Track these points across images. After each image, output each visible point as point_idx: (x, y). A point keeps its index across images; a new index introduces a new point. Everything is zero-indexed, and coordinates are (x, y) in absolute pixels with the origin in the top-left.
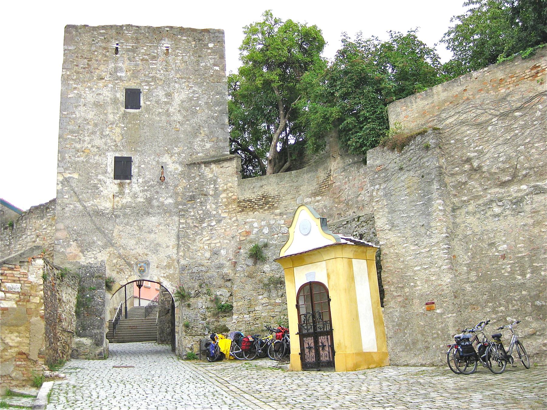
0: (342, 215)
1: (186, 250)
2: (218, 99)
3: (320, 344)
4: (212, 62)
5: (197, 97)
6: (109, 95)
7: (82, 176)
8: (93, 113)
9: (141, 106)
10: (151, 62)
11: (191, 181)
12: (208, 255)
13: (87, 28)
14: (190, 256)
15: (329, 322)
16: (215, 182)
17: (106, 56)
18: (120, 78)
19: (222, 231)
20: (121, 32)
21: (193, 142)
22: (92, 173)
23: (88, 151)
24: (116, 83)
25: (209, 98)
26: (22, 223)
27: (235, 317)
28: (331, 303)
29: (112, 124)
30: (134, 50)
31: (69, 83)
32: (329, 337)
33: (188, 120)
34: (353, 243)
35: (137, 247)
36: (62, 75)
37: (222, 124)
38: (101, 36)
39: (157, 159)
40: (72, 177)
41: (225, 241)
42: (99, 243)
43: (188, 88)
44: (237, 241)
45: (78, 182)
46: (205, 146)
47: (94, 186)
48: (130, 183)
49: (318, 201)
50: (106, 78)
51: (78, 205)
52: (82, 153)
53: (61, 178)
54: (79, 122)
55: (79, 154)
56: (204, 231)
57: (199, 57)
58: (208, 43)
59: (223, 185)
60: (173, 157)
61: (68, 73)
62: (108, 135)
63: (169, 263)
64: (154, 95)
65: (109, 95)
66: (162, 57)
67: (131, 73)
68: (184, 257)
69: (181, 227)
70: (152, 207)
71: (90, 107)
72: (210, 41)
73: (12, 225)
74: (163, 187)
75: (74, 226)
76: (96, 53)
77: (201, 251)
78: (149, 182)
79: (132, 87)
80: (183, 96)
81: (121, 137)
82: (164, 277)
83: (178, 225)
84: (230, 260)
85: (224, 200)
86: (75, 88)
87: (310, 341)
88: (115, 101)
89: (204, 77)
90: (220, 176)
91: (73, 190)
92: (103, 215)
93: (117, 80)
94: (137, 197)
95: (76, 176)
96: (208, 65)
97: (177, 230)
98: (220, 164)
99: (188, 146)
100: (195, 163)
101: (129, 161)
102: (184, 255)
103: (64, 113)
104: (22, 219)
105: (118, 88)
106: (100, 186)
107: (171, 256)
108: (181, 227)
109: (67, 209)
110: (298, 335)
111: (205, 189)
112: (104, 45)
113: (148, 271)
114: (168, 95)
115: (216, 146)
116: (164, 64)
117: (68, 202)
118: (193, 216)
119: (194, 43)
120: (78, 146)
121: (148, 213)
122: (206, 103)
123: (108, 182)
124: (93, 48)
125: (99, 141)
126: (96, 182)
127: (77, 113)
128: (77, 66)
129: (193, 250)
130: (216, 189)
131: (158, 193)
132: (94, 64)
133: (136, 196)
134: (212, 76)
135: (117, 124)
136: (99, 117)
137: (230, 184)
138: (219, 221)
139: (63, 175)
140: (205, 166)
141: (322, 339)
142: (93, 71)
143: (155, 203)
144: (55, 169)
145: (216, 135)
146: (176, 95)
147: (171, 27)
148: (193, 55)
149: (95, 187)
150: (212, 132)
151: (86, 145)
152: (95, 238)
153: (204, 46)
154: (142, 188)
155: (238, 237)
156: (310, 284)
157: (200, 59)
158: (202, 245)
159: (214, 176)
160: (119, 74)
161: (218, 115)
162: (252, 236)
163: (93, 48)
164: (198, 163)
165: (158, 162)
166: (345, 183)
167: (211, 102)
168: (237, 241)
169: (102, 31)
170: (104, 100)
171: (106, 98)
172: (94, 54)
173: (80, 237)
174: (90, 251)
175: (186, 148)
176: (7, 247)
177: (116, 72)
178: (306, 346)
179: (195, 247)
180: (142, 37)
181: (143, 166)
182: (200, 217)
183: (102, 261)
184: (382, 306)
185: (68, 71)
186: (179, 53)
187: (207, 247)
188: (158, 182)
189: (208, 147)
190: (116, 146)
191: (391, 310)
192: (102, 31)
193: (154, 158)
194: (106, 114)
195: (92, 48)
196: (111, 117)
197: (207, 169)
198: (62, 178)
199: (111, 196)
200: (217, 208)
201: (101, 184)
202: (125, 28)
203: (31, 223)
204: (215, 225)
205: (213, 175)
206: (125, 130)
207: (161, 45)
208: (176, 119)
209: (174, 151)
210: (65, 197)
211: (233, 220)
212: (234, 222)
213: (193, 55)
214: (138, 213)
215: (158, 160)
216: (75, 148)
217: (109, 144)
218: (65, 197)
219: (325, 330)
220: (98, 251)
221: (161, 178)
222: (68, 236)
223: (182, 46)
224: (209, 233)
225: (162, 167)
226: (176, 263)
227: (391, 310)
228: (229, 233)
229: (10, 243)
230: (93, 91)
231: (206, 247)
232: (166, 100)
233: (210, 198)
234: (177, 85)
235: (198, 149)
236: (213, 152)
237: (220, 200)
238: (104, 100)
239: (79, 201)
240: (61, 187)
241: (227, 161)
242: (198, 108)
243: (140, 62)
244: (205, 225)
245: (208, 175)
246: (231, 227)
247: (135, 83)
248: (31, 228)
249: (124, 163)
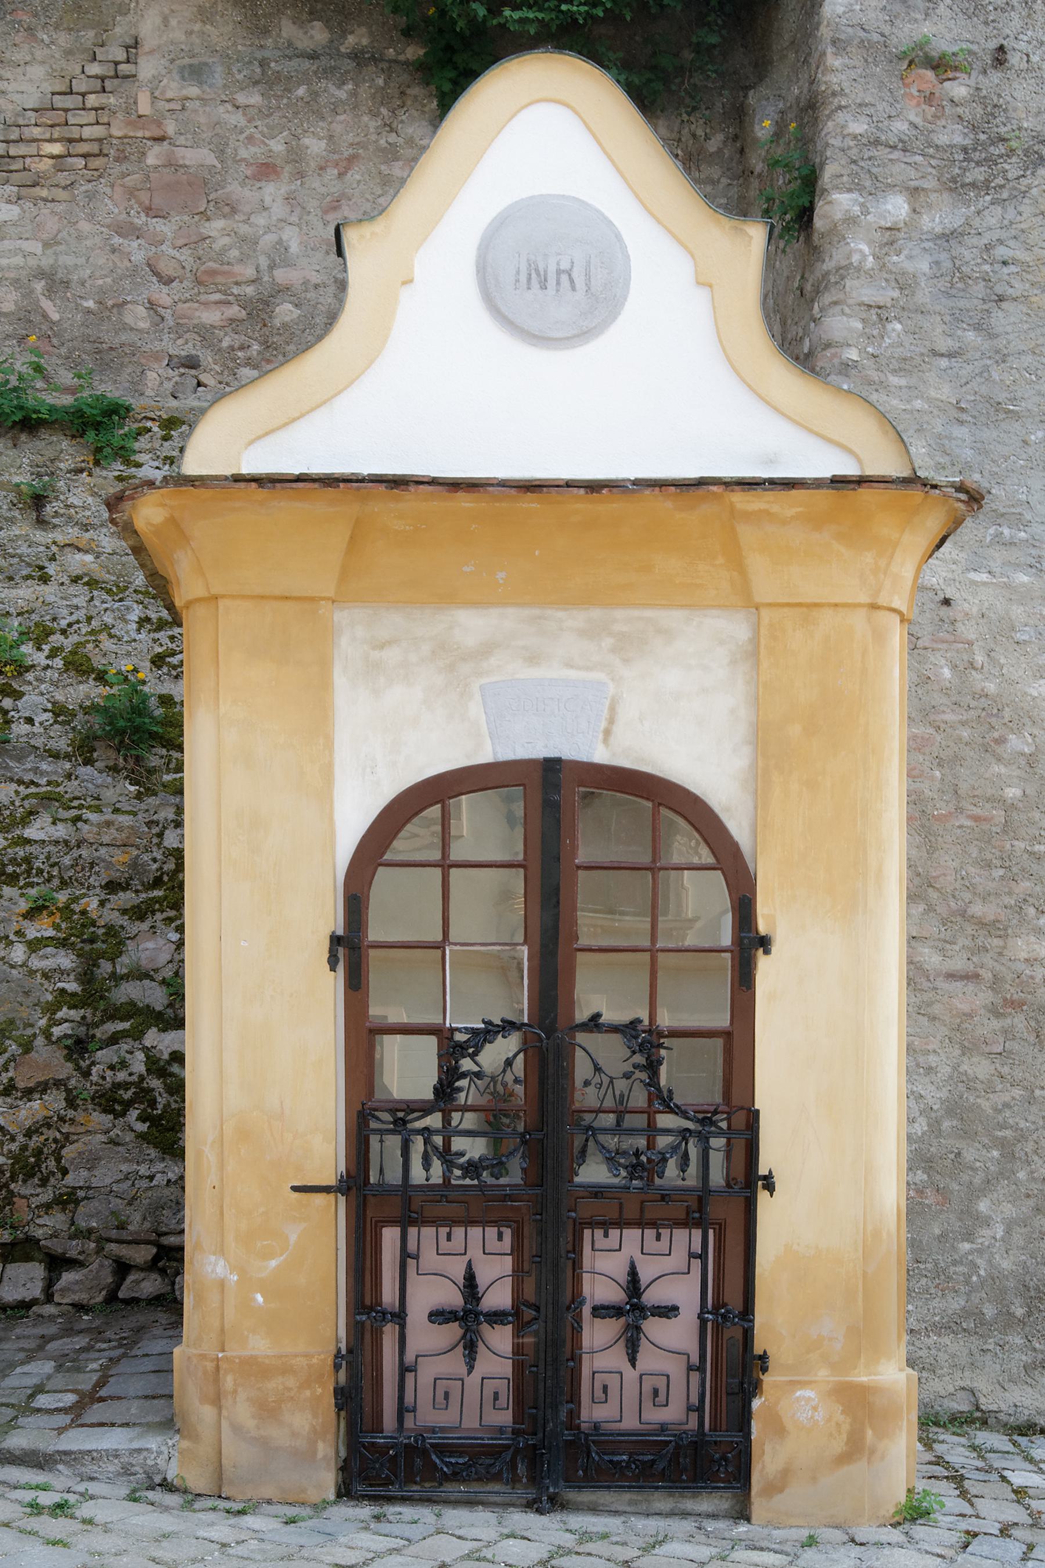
166: (266, 170)
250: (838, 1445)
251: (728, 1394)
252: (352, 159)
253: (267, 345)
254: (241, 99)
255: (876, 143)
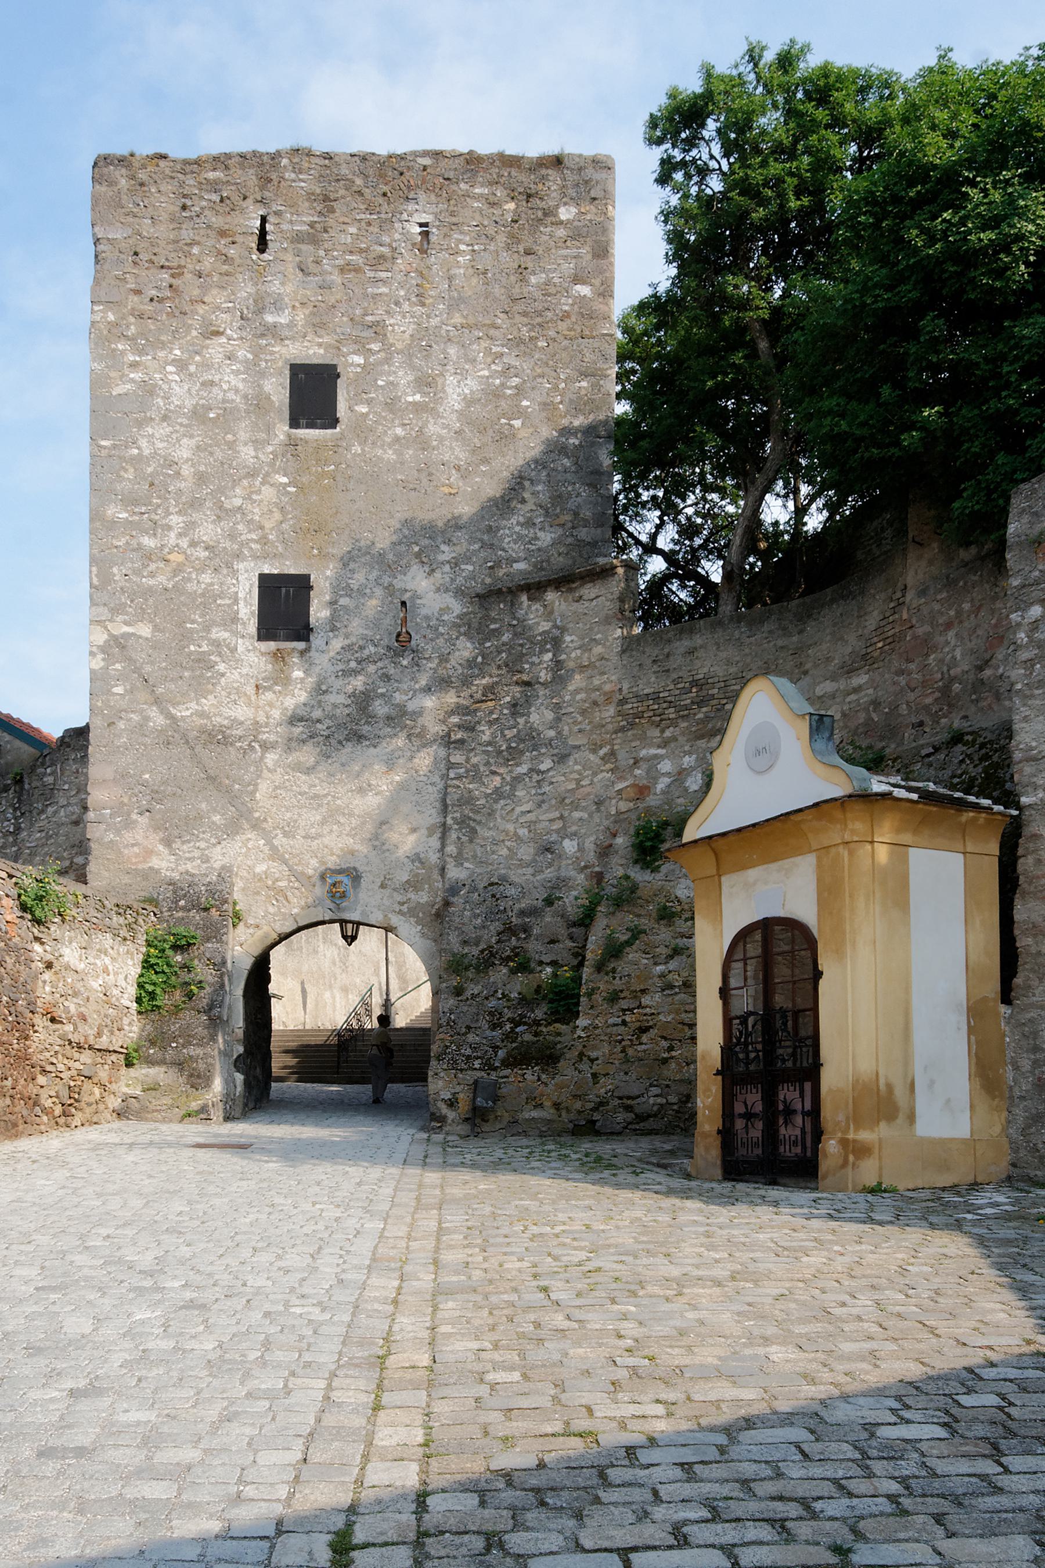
0: (927, 729)
1: (464, 839)
2: (583, 392)
3: (781, 1107)
4: (568, 268)
5: (516, 387)
6: (241, 386)
7: (162, 631)
8: (193, 442)
9: (337, 421)
10: (371, 274)
11: (488, 644)
12: (526, 852)
13: (162, 163)
14: (475, 856)
15: (809, 1042)
16: (557, 643)
17: (227, 259)
18: (272, 331)
19: (570, 787)
20: (274, 176)
21: (498, 529)
22: (193, 622)
23: (180, 558)
24: (261, 347)
25: (556, 388)
26: (45, 774)
27: (582, 1022)
28: (823, 984)
29: (252, 474)
30: (313, 237)
31: (114, 350)
32: (808, 1086)
33: (485, 461)
34: (914, 796)
35: (326, 829)
36: (93, 323)
37: (592, 473)
38: (209, 191)
39: (386, 580)
40: (133, 634)
41: (577, 815)
42: (217, 818)
43: (489, 360)
44: (608, 815)
45: (151, 647)
46: (536, 538)
47: (199, 661)
48: (307, 650)
49: (856, 690)
50: (229, 332)
51: (154, 712)
52: (161, 565)
53: (101, 638)
54: (150, 470)
55: (153, 567)
56: (520, 786)
57: (528, 252)
58: (557, 207)
59: (579, 652)
60: (438, 575)
61: (111, 317)
62: (240, 508)
63: (417, 875)
64: (380, 383)
65: (241, 386)
66: (408, 258)
67: (307, 312)
68: (459, 860)
69: (452, 775)
70: (370, 718)
71: (181, 425)
72: (565, 198)
73: (19, 781)
74: (405, 663)
75: (143, 773)
76: (195, 250)
77: (508, 843)
78: (362, 648)
79: (308, 356)
80: (471, 385)
81: (277, 516)
82: (401, 912)
83: (444, 772)
84: (586, 867)
85: (578, 697)
86: (134, 365)
87: (753, 1099)
88: (259, 404)
89: (539, 320)
90: (571, 625)
91: (137, 670)
92: (225, 741)
93: (263, 335)
94: (325, 692)
95: (145, 630)
96: (556, 280)
97: (441, 785)
98: (571, 590)
99: (481, 540)
100: (499, 592)
101: (302, 584)
102: (460, 853)
103: (104, 443)
104: (43, 764)
105: (266, 361)
106: (218, 659)
107: (422, 856)
108: (452, 775)
109: (121, 725)
110: (720, 1078)
111: (526, 666)
112: (217, 221)
113: (356, 896)
114: (425, 383)
115: (570, 540)
116: (414, 282)
117: (123, 704)
118: (489, 744)
119: (511, 206)
120: (149, 542)
121: (360, 738)
122: (545, 404)
123: (240, 649)
124: (187, 234)
125: (211, 526)
126: (205, 648)
127: (143, 443)
128: (138, 292)
129: (484, 839)
130: (558, 664)
131: (389, 680)
132: (190, 287)
133: (324, 688)
134: (566, 315)
135: (267, 474)
136: (211, 454)
137: (598, 650)
138: (561, 759)
139: (106, 628)
140: (529, 599)
141: (788, 1094)
142: (187, 308)
143: (380, 708)
144: (84, 612)
145: (571, 504)
146: (451, 380)
147: (437, 155)
148: (508, 248)
149: (203, 662)
150: (558, 498)
151: (172, 538)
152: (204, 805)
153: (545, 214)
154: (341, 666)
155: (614, 801)
156: (766, 926)
157: (529, 261)
158: (510, 827)
159: (555, 626)
160: (270, 318)
161: (580, 445)
162: (652, 801)
163: (187, 234)
164: (510, 591)
165: (390, 590)
166: (949, 626)
167: (561, 402)
168: (608, 815)
169: (211, 175)
170: (224, 401)
171: (231, 395)
172: (188, 255)
173: (160, 802)
174: (189, 841)
175: (477, 546)
176: (11, 839)
177: (260, 311)
178: (739, 1108)
179: (491, 833)
180: (342, 192)
181: (343, 601)
182: (509, 748)
183: (223, 867)
184: (1006, 998)
185: (111, 309)
186: (460, 241)
187: (526, 831)
188: (389, 648)
189: (545, 544)
190: (264, 541)
191: (1032, 1014)
192: (211, 175)
193: (380, 577)
194: (231, 445)
195: (184, 232)
196: (247, 453)
197: (536, 606)
198: (106, 636)
199: (250, 690)
200: (558, 719)
201: (220, 655)
202: (285, 161)
203: (67, 773)
204: (548, 770)
205: (550, 624)
206: (289, 493)
207: (405, 216)
208: (446, 457)
209: (441, 557)
210: (115, 690)
211: (602, 752)
212: (602, 759)
213: (508, 248)
214: (328, 737)
215: (391, 585)
216: (140, 547)
217: (243, 537)
218: (115, 690)
219: (798, 1064)
220: (213, 841)
221: (399, 635)
222: (126, 800)
223: (473, 218)
224: (533, 792)
225: (403, 604)
226: (436, 876)
227: (1032, 1014)
228: (588, 789)
229: (18, 829)
230: (191, 375)
231: (523, 832)
232: (418, 397)
233: (541, 693)
234: (452, 351)
235: (515, 549)
236: (561, 559)
237: (567, 698)
238: (224, 401)
239: (157, 701)
240: (102, 664)
241: (592, 581)
242: (517, 423)
243: (336, 278)
244: (523, 769)
245: (538, 624)
246: (595, 774)
247: (320, 345)
248: (66, 787)
249: (288, 592)
250: (841, 1161)
251: (16, 861)
252: (981, 606)
253: (950, 705)
254: (939, 597)
255: (1024, 586)
